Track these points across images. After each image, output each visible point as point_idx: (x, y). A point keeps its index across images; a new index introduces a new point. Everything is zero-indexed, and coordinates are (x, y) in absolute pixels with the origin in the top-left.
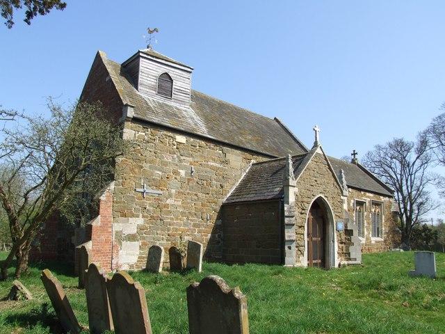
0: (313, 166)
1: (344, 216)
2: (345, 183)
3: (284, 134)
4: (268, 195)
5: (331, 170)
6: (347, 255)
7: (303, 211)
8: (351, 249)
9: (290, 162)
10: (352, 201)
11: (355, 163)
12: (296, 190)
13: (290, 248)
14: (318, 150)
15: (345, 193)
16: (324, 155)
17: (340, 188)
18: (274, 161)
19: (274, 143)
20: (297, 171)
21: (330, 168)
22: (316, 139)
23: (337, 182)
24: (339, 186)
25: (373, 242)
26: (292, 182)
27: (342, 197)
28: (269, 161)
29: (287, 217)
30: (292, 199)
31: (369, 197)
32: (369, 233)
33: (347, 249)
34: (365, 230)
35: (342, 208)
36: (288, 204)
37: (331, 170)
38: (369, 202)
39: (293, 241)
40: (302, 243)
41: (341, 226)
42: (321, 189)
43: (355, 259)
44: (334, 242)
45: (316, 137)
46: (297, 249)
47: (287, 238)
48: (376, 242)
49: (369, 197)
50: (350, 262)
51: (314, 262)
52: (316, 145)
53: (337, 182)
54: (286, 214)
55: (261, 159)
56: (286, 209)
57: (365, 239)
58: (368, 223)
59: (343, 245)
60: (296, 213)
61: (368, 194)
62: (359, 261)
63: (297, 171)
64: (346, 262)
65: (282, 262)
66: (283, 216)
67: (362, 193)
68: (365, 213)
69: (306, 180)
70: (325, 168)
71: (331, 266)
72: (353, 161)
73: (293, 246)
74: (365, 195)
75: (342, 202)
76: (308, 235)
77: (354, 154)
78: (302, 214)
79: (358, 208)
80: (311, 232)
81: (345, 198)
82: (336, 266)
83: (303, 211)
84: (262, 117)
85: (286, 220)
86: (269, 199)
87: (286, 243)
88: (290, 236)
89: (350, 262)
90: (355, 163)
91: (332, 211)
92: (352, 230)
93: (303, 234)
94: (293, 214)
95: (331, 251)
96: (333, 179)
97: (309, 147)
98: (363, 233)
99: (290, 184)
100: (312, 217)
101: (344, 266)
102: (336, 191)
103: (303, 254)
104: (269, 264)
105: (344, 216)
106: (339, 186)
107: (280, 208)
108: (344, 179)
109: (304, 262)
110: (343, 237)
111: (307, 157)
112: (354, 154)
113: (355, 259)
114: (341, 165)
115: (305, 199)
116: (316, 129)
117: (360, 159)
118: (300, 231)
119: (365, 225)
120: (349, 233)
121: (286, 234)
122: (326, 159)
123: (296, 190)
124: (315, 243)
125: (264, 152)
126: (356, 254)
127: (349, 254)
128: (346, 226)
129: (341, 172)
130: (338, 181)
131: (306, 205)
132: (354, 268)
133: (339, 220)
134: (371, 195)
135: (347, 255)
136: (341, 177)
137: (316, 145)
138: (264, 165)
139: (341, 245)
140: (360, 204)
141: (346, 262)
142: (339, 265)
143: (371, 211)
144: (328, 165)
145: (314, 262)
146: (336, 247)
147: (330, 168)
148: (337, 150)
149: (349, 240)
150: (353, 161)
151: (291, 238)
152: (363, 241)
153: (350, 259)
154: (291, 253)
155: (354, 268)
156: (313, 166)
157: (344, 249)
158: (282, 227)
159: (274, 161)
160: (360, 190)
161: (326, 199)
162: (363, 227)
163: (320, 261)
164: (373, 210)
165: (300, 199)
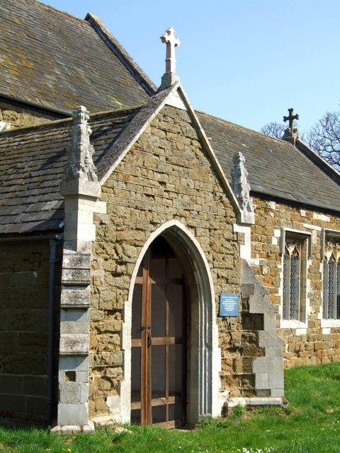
0: (156, 140)
1: (242, 278)
2: (246, 188)
3: (109, 58)
4: (25, 222)
5: (208, 155)
6: (247, 381)
7: (120, 269)
8: (258, 364)
9: (85, 128)
10: (277, 233)
11: (291, 140)
12: (101, 207)
13: (72, 376)
14: (172, 99)
15: (248, 215)
16: (189, 112)
17: (233, 203)
18: (58, 126)
19: (75, 80)
20: (102, 160)
21: (204, 149)
22: (168, 67)
23: (222, 184)
24: (229, 197)
25: (326, 332)
26: (86, 185)
27: (237, 228)
28: (46, 127)
29: (69, 286)
30: (86, 232)
31: (318, 223)
32: (317, 311)
33: (248, 366)
34: (308, 301)
35: (236, 257)
36: (75, 248)
37: (208, 155)
38: (320, 236)
39: (82, 356)
40: (115, 358)
41: (231, 305)
42: (177, 205)
43: (268, 393)
44: (210, 347)
45: (168, 62)
46: (98, 375)
47: (63, 349)
48: (334, 330)
49: (318, 223)
50: (255, 400)
51: (156, 403)
52: (167, 79)
53: (222, 184)
54: (66, 277)
55: (27, 120)
56: (66, 261)
57: (306, 325)
58: (316, 287)
59: (237, 355)
60: (99, 274)
61: (316, 216)
62: (277, 398)
63: (102, 160)
64: (242, 401)
65: (52, 419)
66: (58, 285)
67: (303, 212)
68: (309, 263)
69: (132, 180)
70: (189, 149)
71: (203, 415)
72: (288, 136)
73: (84, 369)
74: (308, 217)
75: (236, 240)
76: (137, 332)
77: (291, 118)
78: (115, 274)
79: (291, 249)
80: (147, 319)
81: (247, 231)
82: (216, 412)
83: (120, 269)
84: (50, 10)
85: (66, 296)
86: (25, 234)
87: (62, 362)
88: (74, 343)
89: (255, 400)
90: (291, 140)
91: (208, 266)
92: (261, 316)
93: (120, 333)
94: (86, 276)
95: (203, 373)
96: (212, 179)
97: (156, 82)
98: (303, 310)
99: (81, 192)
100: (150, 281)
101: (237, 410)
102: (221, 211)
103: (117, 388)
104: (57, 403)
105: (242, 278)
106: (229, 197)
107: (52, 258)
108: (243, 180)
109: (120, 410)
110: (238, 333)
111: (139, 116)
112: (291, 118)
113: (268, 393)
114: (257, 145)
115: (128, 235)
116: (167, 38)
117: (306, 130)
118: (111, 322)
119: (309, 290)
120: (253, 322)
121: (64, 336)
122: (194, 124)
123: (101, 207)
124: (157, 350)
125: (37, 102)
126: (270, 376)
127: (252, 378)
128: (245, 304)
129: (237, 160)
130: (227, 189)
131: (131, 250)
132: (262, 417)
133: (227, 288)
134: (325, 218)
135: (247, 381)
136: (236, 175)
137: (167, 79)
138: (29, 135)
139: (229, 356)
140: (297, 239)
141: (242, 401)
142: (225, 409)
143: (322, 258)
144: (201, 140)
145: (156, 403)
146: (216, 360)
147: (204, 149)
148: (208, 102)
149: (255, 341)
150: (288, 136)
151: (77, 349)
152: (301, 328)
153: (254, 392)
154: (74, 392)
155: (262, 417)
156: (156, 140)
157: (240, 365)
158: (54, 314)
159: (58, 126)
160: (297, 205)
161: (190, 233)
162: (303, 297)
163: (172, 400)
164: (329, 254)
165: (112, 235)
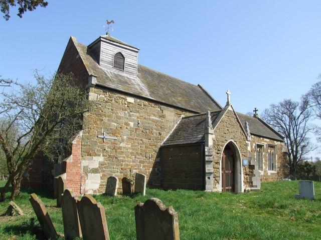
0: (226, 119)
1: (248, 155)
2: (249, 131)
3: (205, 96)
4: (194, 140)
5: (239, 122)
6: (250, 183)
7: (219, 152)
8: (253, 179)
9: (210, 116)
10: (254, 145)
11: (256, 117)
12: (214, 136)
13: (209, 178)
14: (230, 108)
15: (249, 138)
16: (234, 111)
17: (245, 135)
18: (198, 116)
19: (198, 103)
20: (214, 123)
21: (238, 121)
22: (228, 100)
23: (243, 131)
24: (244, 133)
25: (269, 174)
26: (210, 131)
27: (247, 142)
28: (194, 116)
29: (207, 156)
30: (210, 143)
31: (266, 142)
32: (266, 168)
33: (251, 179)
34: (264, 165)
35: (246, 149)
36: (208, 146)
37: (239, 122)
38: (266, 145)
39: (211, 173)
40: (218, 175)
41: (246, 163)
42: (231, 136)
43: (256, 186)
44: (241, 174)
45: (228, 99)
46: (214, 179)
47: (207, 171)
48: (271, 174)
49: (266, 142)
50: (253, 188)
51: (227, 188)
52: (228, 104)
53: (243, 131)
54: (206, 154)
55: (189, 114)
56: (206, 150)
57: (263, 172)
58: (266, 161)
59: (248, 176)
60: (214, 153)
61: (265, 139)
62: (259, 188)
63: (214, 123)
64: (250, 189)
65: (203, 188)
66: (204, 155)
67: (261, 138)
68: (264, 153)
69: (221, 129)
70: (234, 121)
71: (239, 191)
72: (255, 116)
73: (212, 177)
74: (263, 140)
75: (247, 145)
76: (222, 169)
77: (256, 111)
78: (218, 153)
79: (258, 149)
80: (224, 167)
81: (249, 142)
82: (243, 191)
83: (219, 152)
84: (189, 84)
85: (207, 158)
86: (194, 143)
87: (206, 175)
88: (209, 170)
89: (253, 188)
90: (256, 117)
91: (240, 152)
92: (254, 166)
93: (219, 168)
94: (211, 154)
95: (239, 180)
96: (240, 129)
97: (223, 105)
98: (262, 167)
99: (209, 132)
100: (225, 156)
101: (248, 191)
102: (243, 137)
103: (218, 183)
104: (194, 190)
105: (248, 155)
106: (244, 133)
107: (202, 149)
108: (248, 129)
109: (219, 188)
110: (248, 170)
111: (221, 113)
112: (256, 111)
113: (256, 186)
114: (246, 118)
115: (220, 143)
116: (228, 93)
117: (260, 114)
118: (217, 166)
119: (264, 161)
120: (252, 167)
121: (206, 168)
122: (235, 114)
123: (214, 136)
124: (227, 174)
125: (190, 109)
126: (257, 182)
127: (252, 182)
128: (250, 162)
129: (246, 124)
130: (244, 130)
131: (221, 147)
132: (255, 192)
133: (245, 158)
134: (268, 140)
135: (250, 183)
136: (246, 127)
137: (228, 104)
138: (190, 118)
139: (246, 176)
140: (260, 146)
141: (250, 189)
142: (245, 190)
143: (267, 152)
144: (237, 119)
145: (227, 188)
146: (242, 177)
147: (238, 121)
148: (243, 108)
149: (252, 172)
150: (255, 116)
151: (210, 171)
152: (262, 173)
153: (252, 186)
154: (210, 182)
155: (255, 192)
156: (226, 119)
157: (248, 179)
158: (203, 163)
159: (198, 116)
160: (260, 136)
161: (235, 143)
162: (262, 163)
163: (231, 188)
164: (269, 151)
165: (216, 143)
